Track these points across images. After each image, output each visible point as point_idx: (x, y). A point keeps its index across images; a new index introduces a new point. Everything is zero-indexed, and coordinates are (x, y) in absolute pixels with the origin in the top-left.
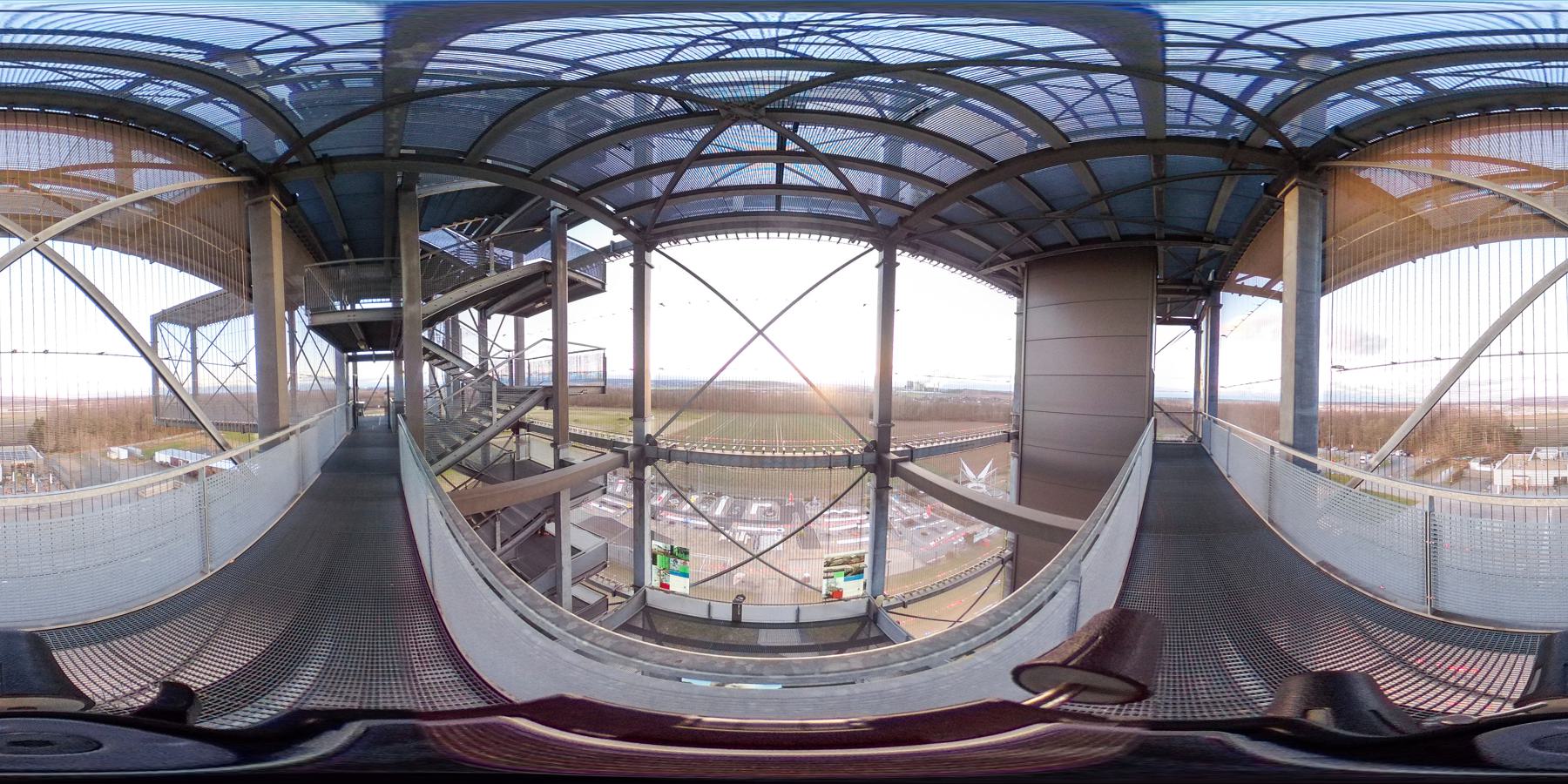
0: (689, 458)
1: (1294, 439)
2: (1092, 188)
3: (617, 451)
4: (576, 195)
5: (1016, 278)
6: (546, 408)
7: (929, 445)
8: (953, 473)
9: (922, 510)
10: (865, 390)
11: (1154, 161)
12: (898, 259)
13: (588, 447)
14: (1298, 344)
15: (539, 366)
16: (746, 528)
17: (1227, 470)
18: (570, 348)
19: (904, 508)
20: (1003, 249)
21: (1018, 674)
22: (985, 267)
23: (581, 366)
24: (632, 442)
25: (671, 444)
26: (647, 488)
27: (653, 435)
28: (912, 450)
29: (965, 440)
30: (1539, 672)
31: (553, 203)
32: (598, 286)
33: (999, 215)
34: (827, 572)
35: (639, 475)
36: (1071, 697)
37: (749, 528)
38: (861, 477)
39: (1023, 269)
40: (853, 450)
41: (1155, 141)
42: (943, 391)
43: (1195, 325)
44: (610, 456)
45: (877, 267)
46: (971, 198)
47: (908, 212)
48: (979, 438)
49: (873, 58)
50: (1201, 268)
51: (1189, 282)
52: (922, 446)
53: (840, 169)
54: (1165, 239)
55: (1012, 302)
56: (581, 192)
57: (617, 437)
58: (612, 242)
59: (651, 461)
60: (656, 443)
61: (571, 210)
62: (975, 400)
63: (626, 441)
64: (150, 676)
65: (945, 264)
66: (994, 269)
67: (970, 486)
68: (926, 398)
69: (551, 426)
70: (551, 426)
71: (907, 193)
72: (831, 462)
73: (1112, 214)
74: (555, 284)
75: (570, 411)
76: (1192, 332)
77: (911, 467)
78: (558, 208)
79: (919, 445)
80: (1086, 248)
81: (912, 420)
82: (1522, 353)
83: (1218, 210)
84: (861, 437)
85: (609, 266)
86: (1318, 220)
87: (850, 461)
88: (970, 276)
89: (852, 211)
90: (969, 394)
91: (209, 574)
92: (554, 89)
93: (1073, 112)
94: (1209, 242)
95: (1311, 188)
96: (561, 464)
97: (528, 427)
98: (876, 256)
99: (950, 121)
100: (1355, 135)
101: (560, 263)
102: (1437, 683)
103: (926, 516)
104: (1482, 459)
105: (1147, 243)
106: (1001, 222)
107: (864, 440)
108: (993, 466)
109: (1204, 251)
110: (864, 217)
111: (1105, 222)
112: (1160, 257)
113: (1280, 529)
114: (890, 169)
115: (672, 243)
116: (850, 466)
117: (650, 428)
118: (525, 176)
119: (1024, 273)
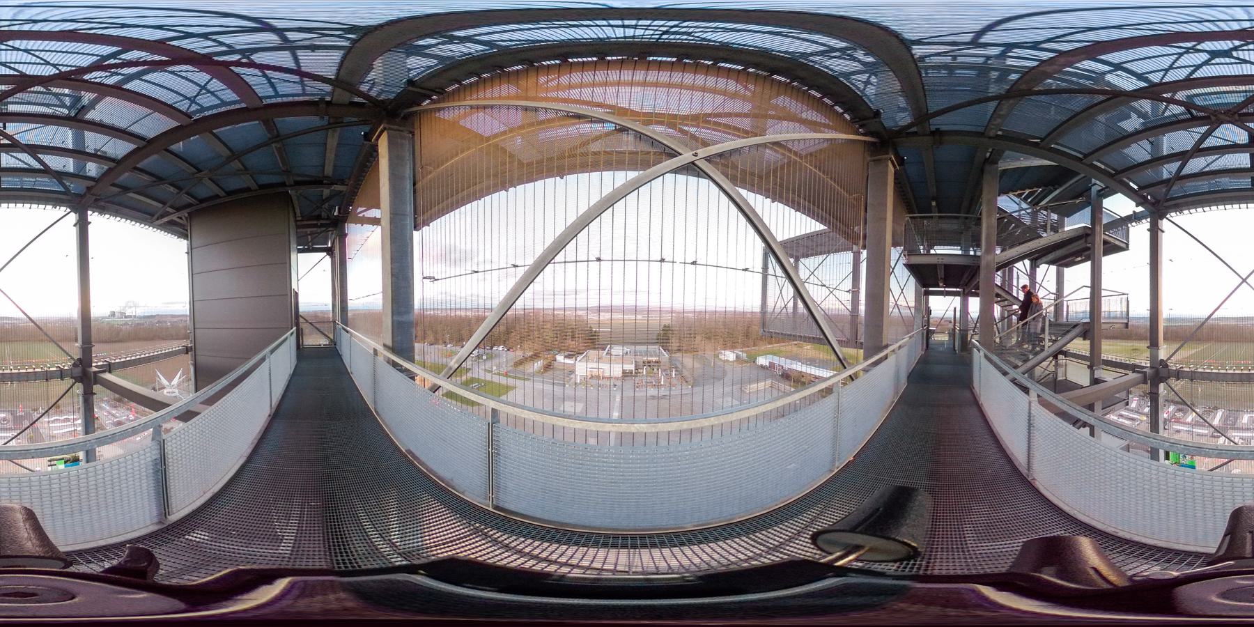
0: (1193, 376)
1: (393, 342)
2: (226, 152)
3: (1138, 372)
4: (1111, 176)
5: (184, 226)
6: (1084, 339)
7: (123, 360)
8: (152, 383)
9: (128, 413)
10: (70, 320)
11: (264, 125)
12: (90, 219)
13: (1114, 369)
14: (393, 260)
15: (1077, 306)
16: (1239, 434)
17: (350, 368)
18: (1104, 293)
19: (114, 412)
20: (168, 204)
21: (815, 538)
22: (158, 219)
23: (1111, 306)
24: (1149, 365)
25: (1179, 366)
26: (1161, 401)
27: (1165, 359)
28: (110, 364)
29: (152, 354)
30: (1229, 537)
31: (1094, 181)
32: (1124, 246)
33: (159, 179)
34: (50, 461)
35: (1154, 391)
36: (858, 557)
37: (1241, 434)
38: (71, 387)
39: (186, 218)
40: (64, 366)
41: (256, 109)
42: (140, 318)
43: (330, 251)
44: (1132, 376)
45: (74, 226)
46: (136, 168)
47: (92, 183)
48: (163, 352)
49: (17, 71)
50: (326, 205)
51: (319, 217)
52: (117, 361)
53: (39, 155)
54: (295, 185)
55: (183, 244)
56: (1116, 174)
57: (1137, 362)
58: (1134, 212)
59: (1163, 379)
60: (1167, 366)
61: (1107, 187)
62: (165, 322)
63: (1144, 365)
64: (764, 546)
65: (127, 219)
66: (166, 219)
67: (165, 391)
68: (126, 324)
69: (1088, 354)
70: (1088, 354)
71: (92, 169)
72: (47, 376)
73: (246, 169)
74: (1094, 244)
75: (1102, 343)
76: (328, 257)
77: (108, 376)
78: (1097, 185)
79: (115, 360)
80: (234, 197)
81: (115, 342)
82: (599, 260)
83: (330, 156)
84: (70, 356)
85: (1131, 229)
86: (408, 156)
87: (62, 374)
88: (147, 227)
89: (45, 183)
90: (160, 318)
91: (836, 471)
92: (1116, 97)
93: (206, 89)
94: (328, 184)
95: (399, 130)
96: (1095, 381)
97: (1066, 354)
98: (73, 217)
99: (108, 110)
100: (431, 84)
101: (1098, 228)
102: (529, 558)
103: (132, 417)
104: (567, 353)
105: (281, 189)
106: (162, 184)
107: (72, 358)
108: (183, 374)
109: (326, 192)
110: (61, 189)
111: (242, 176)
112: (294, 198)
113: (383, 421)
114: (78, 153)
115: (1178, 213)
116: (62, 379)
117: (1163, 354)
118: (1079, 160)
119: (187, 221)
